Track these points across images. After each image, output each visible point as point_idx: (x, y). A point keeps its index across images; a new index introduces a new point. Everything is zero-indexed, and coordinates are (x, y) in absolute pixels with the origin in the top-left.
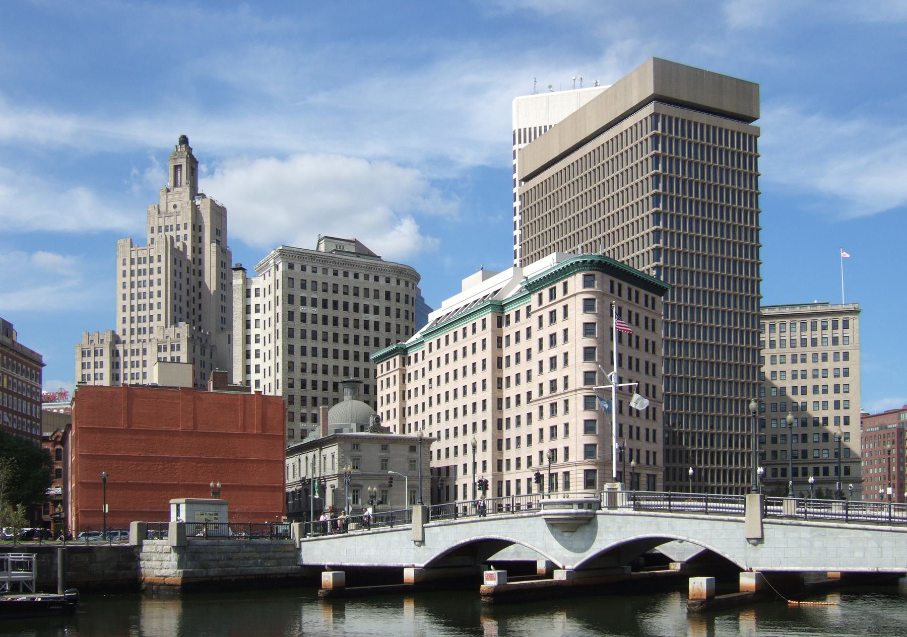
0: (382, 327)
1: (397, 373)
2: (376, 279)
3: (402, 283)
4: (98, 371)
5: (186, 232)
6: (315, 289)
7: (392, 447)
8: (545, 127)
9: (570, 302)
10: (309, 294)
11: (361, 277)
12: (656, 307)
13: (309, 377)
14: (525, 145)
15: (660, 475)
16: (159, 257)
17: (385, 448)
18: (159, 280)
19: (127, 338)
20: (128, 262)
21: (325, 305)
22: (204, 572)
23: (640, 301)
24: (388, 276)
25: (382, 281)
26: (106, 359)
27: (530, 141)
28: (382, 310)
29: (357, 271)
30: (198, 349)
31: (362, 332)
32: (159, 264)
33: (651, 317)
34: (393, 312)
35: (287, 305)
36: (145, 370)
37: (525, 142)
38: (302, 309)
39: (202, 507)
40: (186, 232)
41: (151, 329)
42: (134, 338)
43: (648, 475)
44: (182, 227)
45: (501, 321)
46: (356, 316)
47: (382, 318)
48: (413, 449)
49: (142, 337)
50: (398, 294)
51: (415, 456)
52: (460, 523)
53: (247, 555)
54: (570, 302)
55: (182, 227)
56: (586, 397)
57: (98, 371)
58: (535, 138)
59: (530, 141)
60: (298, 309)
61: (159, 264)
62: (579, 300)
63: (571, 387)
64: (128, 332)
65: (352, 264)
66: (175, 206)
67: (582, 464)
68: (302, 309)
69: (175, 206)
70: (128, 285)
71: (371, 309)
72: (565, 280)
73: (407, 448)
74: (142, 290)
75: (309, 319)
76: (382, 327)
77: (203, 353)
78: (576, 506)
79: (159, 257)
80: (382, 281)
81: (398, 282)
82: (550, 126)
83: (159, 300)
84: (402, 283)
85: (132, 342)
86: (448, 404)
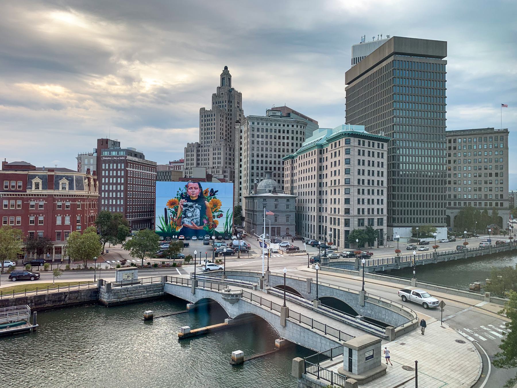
0: (290, 145)
1: (290, 166)
2: (288, 126)
3: (299, 127)
4: (192, 157)
5: (226, 104)
6: (263, 131)
7: (279, 200)
8: (363, 57)
9: (341, 149)
10: (260, 133)
11: (282, 125)
12: (384, 147)
13: (260, 165)
14: (354, 65)
15: (385, 219)
16: (215, 114)
17: (276, 200)
18: (214, 123)
19: (203, 145)
20: (204, 116)
21: (267, 137)
22: (119, 300)
23: (375, 146)
24: (293, 124)
25: (290, 126)
26: (195, 153)
27: (356, 63)
28: (290, 138)
29: (280, 123)
30: (228, 149)
31: (282, 147)
32: (214, 117)
33: (380, 152)
34: (295, 138)
35: (251, 138)
36: (209, 157)
37: (354, 64)
38: (257, 139)
39: (126, 272)
40: (226, 104)
41: (211, 142)
42: (205, 145)
43: (378, 219)
44: (224, 102)
45: (321, 152)
46: (279, 141)
47: (290, 141)
48: (288, 200)
49: (208, 144)
50: (297, 131)
51: (289, 203)
52: (205, 290)
53: (139, 291)
54: (341, 149)
55: (224, 102)
56: (345, 189)
57: (192, 157)
58: (358, 62)
59: (356, 63)
60: (256, 139)
61: (214, 117)
62: (344, 149)
63: (340, 184)
64: (203, 143)
65: (278, 121)
66: (222, 94)
67: (344, 216)
68: (257, 139)
69: (222, 94)
70: (203, 125)
71: (286, 138)
72: (335, 142)
73: (286, 200)
74: (208, 127)
75: (260, 143)
76: (290, 145)
77: (230, 150)
78: (230, 296)
79: (215, 114)
80: (290, 126)
81: (297, 127)
82: (365, 56)
83: (214, 131)
84: (299, 127)
85: (205, 146)
86: (307, 181)
